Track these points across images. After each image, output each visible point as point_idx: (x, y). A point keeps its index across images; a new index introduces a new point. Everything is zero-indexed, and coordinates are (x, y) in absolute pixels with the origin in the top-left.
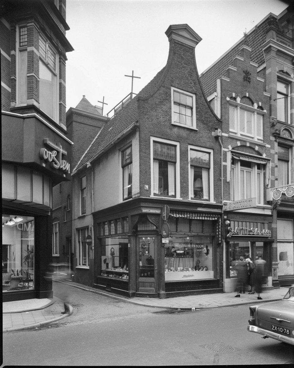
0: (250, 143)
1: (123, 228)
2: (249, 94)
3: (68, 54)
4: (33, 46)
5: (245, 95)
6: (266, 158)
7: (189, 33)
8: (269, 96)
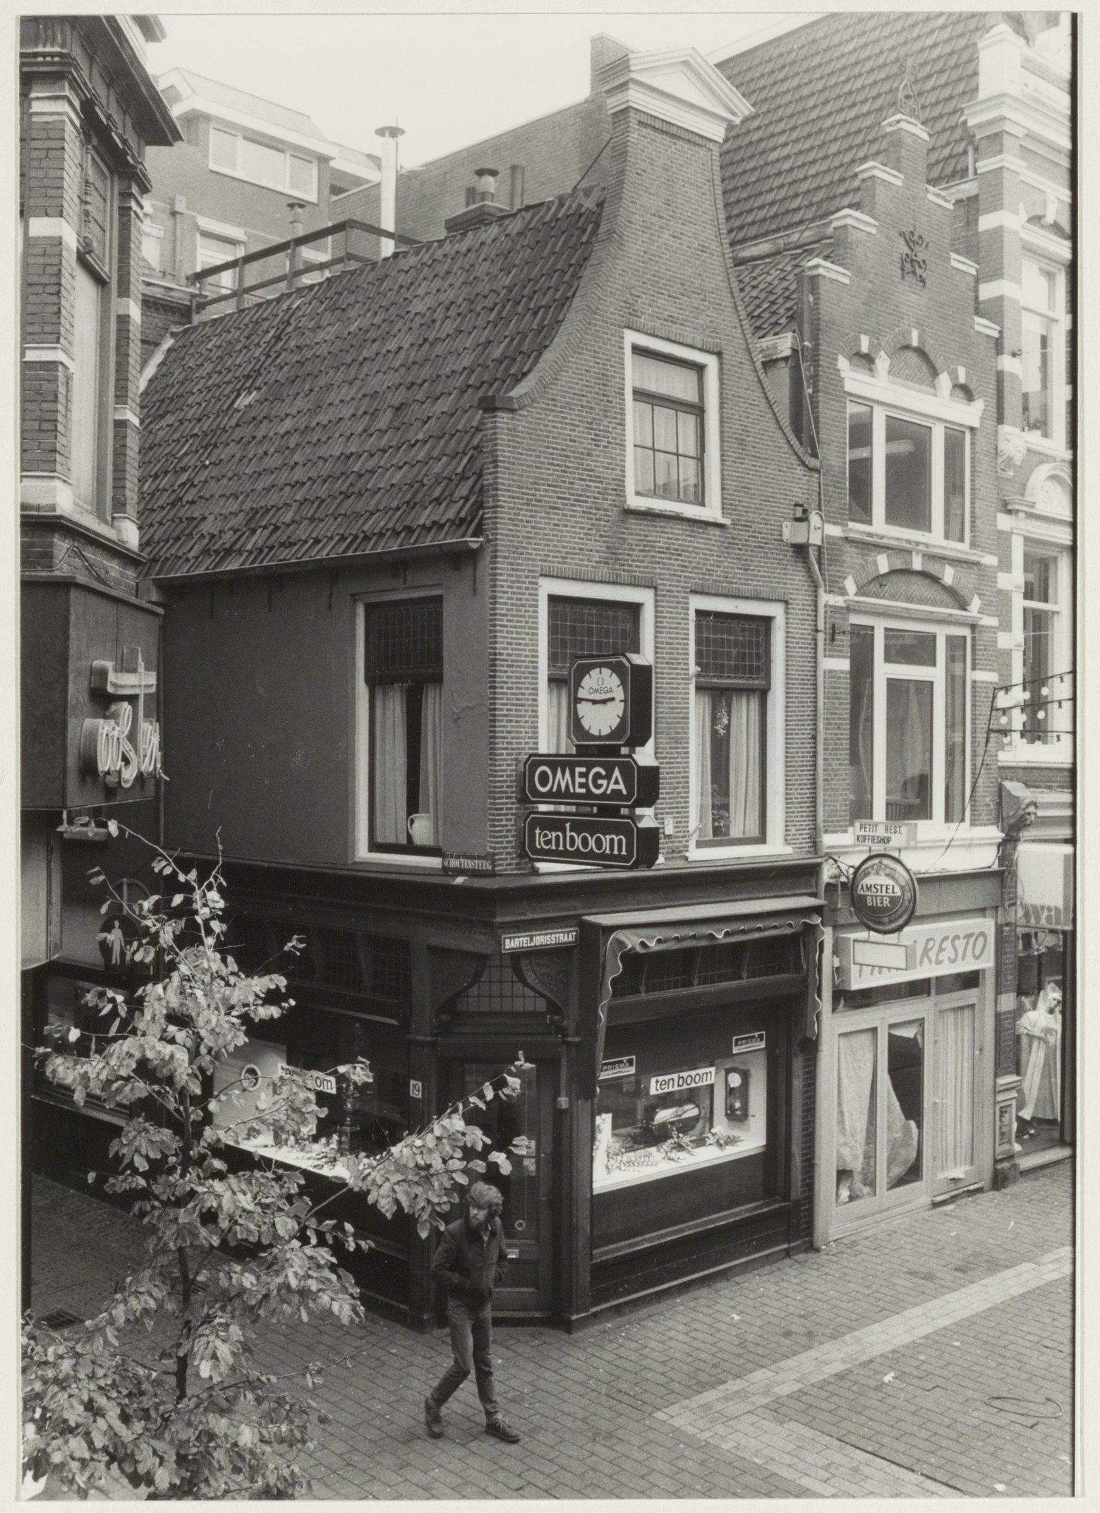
2: (920, 338)
3: (154, 159)
4: (61, 216)
5: (907, 343)
7: (693, 79)
8: (997, 335)
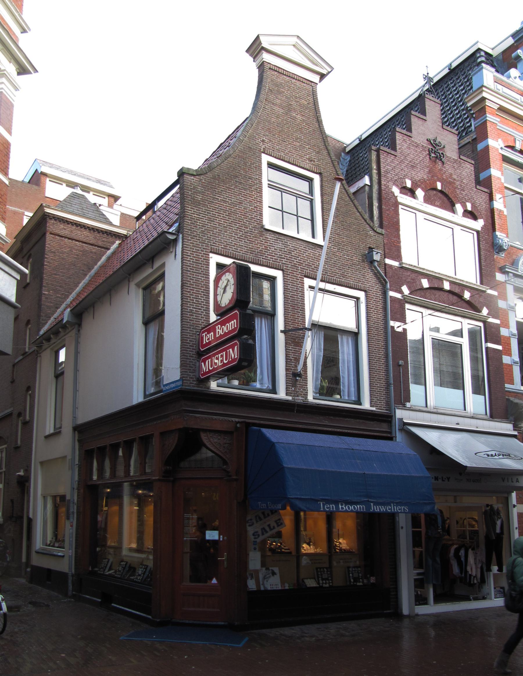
0: (451, 283)
1: (142, 464)
6: (397, 420)
